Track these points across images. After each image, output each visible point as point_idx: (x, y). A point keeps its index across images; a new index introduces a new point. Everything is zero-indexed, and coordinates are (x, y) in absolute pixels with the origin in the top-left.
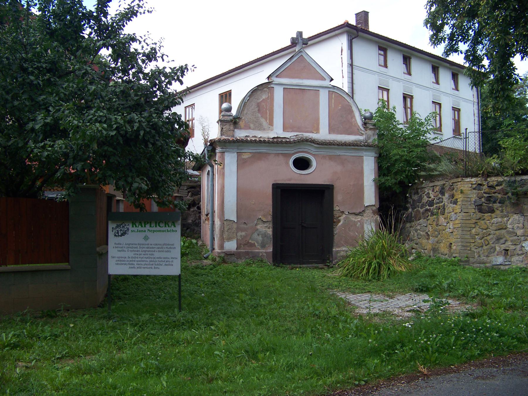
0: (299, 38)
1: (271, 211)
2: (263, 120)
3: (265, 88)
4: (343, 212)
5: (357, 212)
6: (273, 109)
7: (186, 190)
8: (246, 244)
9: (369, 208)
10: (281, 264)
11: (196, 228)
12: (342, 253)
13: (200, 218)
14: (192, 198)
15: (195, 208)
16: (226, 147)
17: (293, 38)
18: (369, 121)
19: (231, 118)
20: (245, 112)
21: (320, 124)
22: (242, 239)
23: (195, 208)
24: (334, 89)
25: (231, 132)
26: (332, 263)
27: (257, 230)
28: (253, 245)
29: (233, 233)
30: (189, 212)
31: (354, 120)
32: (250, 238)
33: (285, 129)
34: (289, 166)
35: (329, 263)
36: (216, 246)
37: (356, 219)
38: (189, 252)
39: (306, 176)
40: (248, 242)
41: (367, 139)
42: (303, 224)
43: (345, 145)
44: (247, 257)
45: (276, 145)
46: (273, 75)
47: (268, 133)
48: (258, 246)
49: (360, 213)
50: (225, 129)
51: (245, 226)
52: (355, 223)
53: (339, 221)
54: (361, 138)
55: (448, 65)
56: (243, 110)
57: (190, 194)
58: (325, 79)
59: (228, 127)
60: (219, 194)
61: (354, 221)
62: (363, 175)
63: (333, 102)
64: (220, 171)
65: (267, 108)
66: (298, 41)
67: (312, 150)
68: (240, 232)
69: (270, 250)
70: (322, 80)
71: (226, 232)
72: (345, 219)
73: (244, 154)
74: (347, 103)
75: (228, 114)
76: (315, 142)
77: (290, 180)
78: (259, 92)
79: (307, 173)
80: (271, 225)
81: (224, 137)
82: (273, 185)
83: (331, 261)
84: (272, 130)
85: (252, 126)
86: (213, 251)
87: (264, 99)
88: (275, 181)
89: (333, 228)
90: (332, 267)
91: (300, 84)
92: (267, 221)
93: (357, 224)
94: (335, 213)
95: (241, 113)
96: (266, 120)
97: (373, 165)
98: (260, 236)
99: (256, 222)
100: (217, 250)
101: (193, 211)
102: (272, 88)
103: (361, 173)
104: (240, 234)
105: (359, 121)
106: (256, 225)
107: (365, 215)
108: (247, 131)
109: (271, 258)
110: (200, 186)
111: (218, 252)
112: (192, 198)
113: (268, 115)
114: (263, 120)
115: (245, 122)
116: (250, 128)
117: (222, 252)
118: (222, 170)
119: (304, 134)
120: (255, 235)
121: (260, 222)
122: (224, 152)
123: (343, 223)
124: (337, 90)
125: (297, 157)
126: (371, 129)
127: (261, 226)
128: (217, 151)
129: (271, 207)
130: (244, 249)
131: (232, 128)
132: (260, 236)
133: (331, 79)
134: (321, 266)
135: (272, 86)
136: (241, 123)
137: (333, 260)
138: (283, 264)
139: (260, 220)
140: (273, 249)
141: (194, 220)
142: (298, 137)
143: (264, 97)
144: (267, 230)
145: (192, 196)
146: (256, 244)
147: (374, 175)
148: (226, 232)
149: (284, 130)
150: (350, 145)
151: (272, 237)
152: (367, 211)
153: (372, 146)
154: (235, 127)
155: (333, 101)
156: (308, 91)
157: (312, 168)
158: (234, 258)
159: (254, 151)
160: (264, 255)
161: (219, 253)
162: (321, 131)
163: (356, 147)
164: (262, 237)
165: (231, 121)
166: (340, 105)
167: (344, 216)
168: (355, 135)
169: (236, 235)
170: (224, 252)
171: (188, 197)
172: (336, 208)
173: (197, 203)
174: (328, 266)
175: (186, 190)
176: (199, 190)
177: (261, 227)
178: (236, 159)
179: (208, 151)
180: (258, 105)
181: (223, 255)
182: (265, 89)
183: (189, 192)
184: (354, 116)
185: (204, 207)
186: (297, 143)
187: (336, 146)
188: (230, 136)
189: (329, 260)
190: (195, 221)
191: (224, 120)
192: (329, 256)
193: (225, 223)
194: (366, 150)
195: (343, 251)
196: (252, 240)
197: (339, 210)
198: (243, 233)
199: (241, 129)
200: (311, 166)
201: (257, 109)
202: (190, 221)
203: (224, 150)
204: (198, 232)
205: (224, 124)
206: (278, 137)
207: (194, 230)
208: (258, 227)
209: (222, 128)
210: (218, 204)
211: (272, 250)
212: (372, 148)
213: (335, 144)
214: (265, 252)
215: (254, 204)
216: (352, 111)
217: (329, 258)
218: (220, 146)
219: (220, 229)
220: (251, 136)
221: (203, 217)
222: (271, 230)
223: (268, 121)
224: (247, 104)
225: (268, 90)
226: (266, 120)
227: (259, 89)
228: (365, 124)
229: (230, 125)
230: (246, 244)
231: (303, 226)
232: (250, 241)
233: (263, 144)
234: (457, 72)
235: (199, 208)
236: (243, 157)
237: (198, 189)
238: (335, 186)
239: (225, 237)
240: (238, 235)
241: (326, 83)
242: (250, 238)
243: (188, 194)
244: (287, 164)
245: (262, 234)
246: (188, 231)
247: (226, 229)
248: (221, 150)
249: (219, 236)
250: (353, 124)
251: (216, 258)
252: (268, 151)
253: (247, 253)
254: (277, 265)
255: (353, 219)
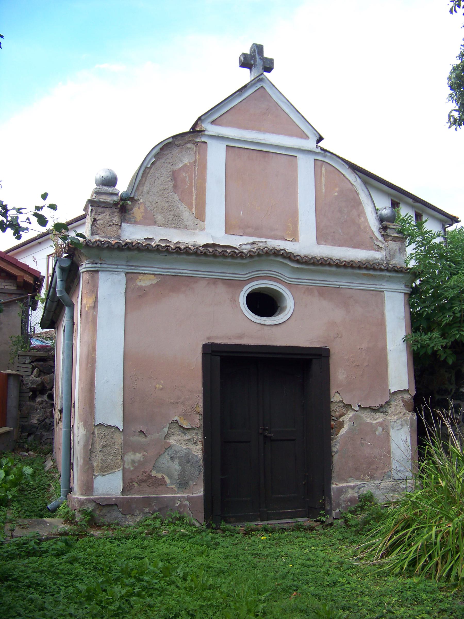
0: (257, 56)
1: (201, 404)
2: (182, 208)
3: (190, 142)
4: (348, 406)
5: (377, 404)
6: (205, 188)
7: (30, 363)
8: (144, 481)
9: (399, 396)
10: (223, 523)
11: (45, 434)
12: (351, 494)
13: (52, 416)
14: (39, 379)
15: (45, 398)
16: (100, 259)
17: (244, 55)
18: (390, 224)
19: (115, 198)
20: (146, 188)
21: (300, 223)
22: (136, 468)
23: (45, 398)
24: (325, 156)
25: (114, 228)
26: (331, 515)
27: (170, 447)
28: (162, 482)
29: (115, 454)
30: (32, 404)
31: (362, 219)
32: (154, 467)
33: (229, 229)
34: (238, 306)
35: (324, 516)
36: (76, 483)
37: (373, 419)
38: (14, 496)
39: (274, 329)
40: (150, 477)
41: (388, 258)
42: (266, 433)
43: (352, 267)
44: (147, 510)
45: (211, 259)
46: (205, 119)
47: (194, 234)
48: (171, 484)
49: (382, 406)
50: (101, 221)
51: (142, 439)
52: (373, 428)
53: (341, 425)
54: (378, 256)
55: (410, 201)
56: (141, 184)
57: (35, 371)
58: (307, 137)
59: (108, 217)
60: (84, 365)
61: (371, 424)
62: (385, 329)
63: (323, 182)
64: (87, 313)
65: (191, 182)
66: (255, 61)
67: (287, 275)
68: (130, 454)
69: (199, 492)
70: (301, 137)
71: (99, 454)
72: (353, 420)
73: (140, 277)
74: (350, 186)
75: (110, 190)
76: (292, 257)
77: (240, 337)
78: (176, 151)
79: (275, 322)
80: (200, 437)
81: (97, 238)
82: (205, 347)
83: (329, 512)
84: (203, 229)
85: (159, 218)
86: (69, 495)
87: (185, 166)
88: (209, 338)
89: (331, 440)
90: (331, 525)
91: (259, 141)
92: (192, 428)
93: (377, 429)
94: (333, 407)
95: (137, 189)
96: (191, 209)
97: (403, 310)
98: (176, 461)
99: (166, 430)
100: (77, 495)
101: (41, 403)
102: (204, 145)
103: (382, 324)
104: (130, 457)
105: (374, 225)
106: (167, 436)
107: (390, 411)
108: (149, 228)
109: (202, 510)
110: (53, 358)
111: (79, 501)
112: (39, 379)
113: (194, 197)
114: (182, 208)
115: (146, 209)
116: (155, 223)
117: (89, 501)
118: (91, 312)
119: (268, 240)
120: (165, 460)
121: (175, 430)
122: (97, 271)
123: (350, 429)
124: (331, 159)
125: (250, 290)
126: (395, 239)
127: (179, 438)
128: (82, 269)
129: (201, 395)
130: (139, 492)
131: (116, 219)
132: (176, 461)
133: (318, 136)
134: (304, 521)
135: (203, 139)
136: (135, 210)
137: (331, 510)
138: (227, 522)
139: (176, 426)
140: (205, 490)
141: (41, 419)
142: (255, 246)
143: (186, 161)
144: (191, 446)
145: (39, 376)
146: (168, 481)
147: (404, 329)
148: (99, 454)
149: (227, 232)
150: (359, 268)
151: (201, 462)
152: (393, 403)
153: (401, 272)
154: (124, 220)
155: (323, 179)
156: (274, 155)
157: (286, 312)
158: (116, 514)
159: (163, 271)
160: (185, 505)
161: (82, 503)
162: (302, 236)
163: (371, 272)
164: (180, 465)
165: (116, 204)
166: (337, 189)
167: (351, 414)
168: (367, 248)
169: (122, 459)
170: (94, 501)
171: (32, 377)
172: (335, 398)
173: (48, 387)
174: (323, 522)
175: (30, 363)
176: (52, 364)
177: (179, 441)
178: (124, 287)
179: (62, 269)
180: (174, 176)
181: (90, 507)
182: (189, 145)
183: (33, 368)
184: (362, 213)
185: (58, 396)
186: (256, 259)
187: (334, 269)
188: (110, 237)
189: (324, 509)
190: (44, 420)
191: (99, 201)
192: (324, 500)
193: (96, 432)
194: (389, 279)
195: (353, 488)
196: (158, 472)
197: (342, 401)
198: (138, 456)
199: (135, 223)
200: (283, 309)
201: (171, 184)
202: (35, 421)
203: (97, 266)
204: (49, 440)
205: (100, 210)
206: (214, 245)
207: (42, 436)
208: (172, 441)
209: (95, 220)
210: (81, 389)
211: (202, 493)
212: (401, 275)
213: (332, 263)
214: (188, 499)
215: (162, 389)
216: (359, 203)
217: (324, 504)
218: (88, 258)
219: (85, 446)
220: (157, 239)
221: (56, 415)
222: (200, 447)
223: (194, 210)
224: (151, 172)
225: (193, 147)
226: (191, 209)
227: (177, 143)
228: (385, 228)
229: (113, 213)
230: (144, 481)
231: (265, 437)
232: (154, 474)
233: (184, 257)
234: (421, 212)
235: (51, 397)
236: (139, 284)
237: (50, 363)
238: (332, 352)
239: (95, 464)
240: (125, 459)
241: (310, 144)
242: (154, 467)
243: (32, 372)
244: (235, 301)
245: (180, 458)
246: (31, 438)
247: (98, 447)
248: (90, 265)
249: (81, 462)
250: (362, 227)
251: (74, 515)
252: (194, 274)
253: (147, 501)
254: (214, 526)
255: (369, 420)
